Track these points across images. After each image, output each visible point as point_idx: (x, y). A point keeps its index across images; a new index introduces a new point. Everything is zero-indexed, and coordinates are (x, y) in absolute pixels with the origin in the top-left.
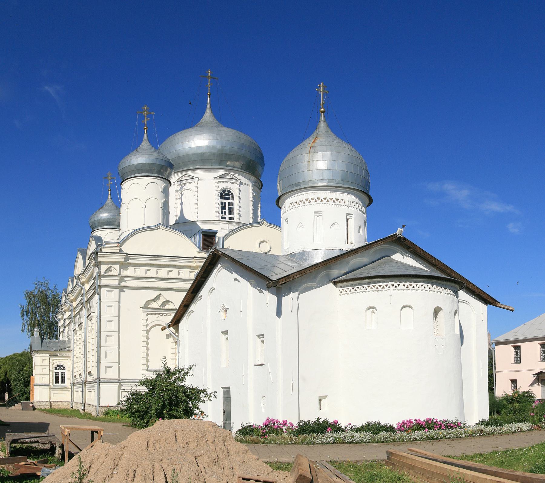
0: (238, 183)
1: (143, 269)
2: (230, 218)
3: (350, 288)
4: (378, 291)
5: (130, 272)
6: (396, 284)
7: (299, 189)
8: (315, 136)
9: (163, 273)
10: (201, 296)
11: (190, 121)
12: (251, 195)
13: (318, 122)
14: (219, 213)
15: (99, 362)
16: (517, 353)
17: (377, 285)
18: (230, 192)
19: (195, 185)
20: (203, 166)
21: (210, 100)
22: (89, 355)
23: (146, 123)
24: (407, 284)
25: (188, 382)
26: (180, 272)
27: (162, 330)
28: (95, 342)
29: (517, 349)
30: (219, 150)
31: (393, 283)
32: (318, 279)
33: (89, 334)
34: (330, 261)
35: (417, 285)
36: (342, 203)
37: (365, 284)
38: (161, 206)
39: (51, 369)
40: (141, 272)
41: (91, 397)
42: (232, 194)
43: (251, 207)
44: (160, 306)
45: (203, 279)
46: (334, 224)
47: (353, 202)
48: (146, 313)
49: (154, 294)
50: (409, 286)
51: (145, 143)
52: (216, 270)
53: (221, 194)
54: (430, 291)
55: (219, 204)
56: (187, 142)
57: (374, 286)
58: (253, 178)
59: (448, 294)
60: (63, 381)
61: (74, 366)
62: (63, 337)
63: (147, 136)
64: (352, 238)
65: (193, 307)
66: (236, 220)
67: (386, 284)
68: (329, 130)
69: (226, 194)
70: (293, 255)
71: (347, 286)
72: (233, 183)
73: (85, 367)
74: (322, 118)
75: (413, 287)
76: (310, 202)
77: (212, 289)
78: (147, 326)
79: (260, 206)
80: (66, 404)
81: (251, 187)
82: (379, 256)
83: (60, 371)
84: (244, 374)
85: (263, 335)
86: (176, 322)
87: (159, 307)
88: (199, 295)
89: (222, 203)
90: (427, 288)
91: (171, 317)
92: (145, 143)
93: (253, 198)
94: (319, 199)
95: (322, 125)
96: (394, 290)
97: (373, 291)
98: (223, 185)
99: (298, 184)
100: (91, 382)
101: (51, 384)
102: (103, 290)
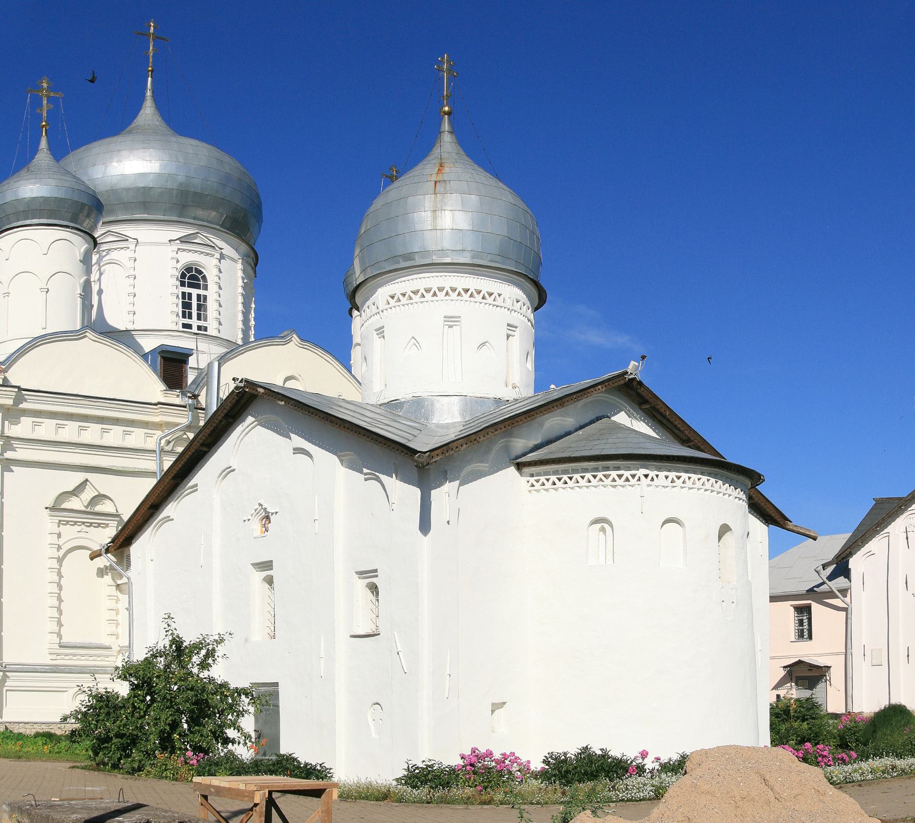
0: (217, 255)
1: (51, 423)
2: (199, 328)
3: (553, 478)
4: (614, 487)
5: (23, 428)
6: (652, 474)
7: (396, 270)
8: (437, 161)
9: (92, 434)
10: (196, 485)
11: (113, 122)
12: (240, 283)
13: (438, 132)
14: (177, 315)
16: (801, 623)
17: (614, 474)
18: (200, 272)
19: (128, 253)
20: (146, 216)
21: (152, 82)
23: (45, 114)
24: (672, 475)
25: (219, 672)
26: (126, 433)
27: (92, 559)
29: (804, 611)
30: (181, 184)
31: (646, 472)
32: (492, 456)
34: (514, 421)
35: (689, 478)
36: (499, 302)
37: (586, 470)
38: (79, 291)
40: (47, 429)
42: (204, 278)
43: (240, 307)
44: (87, 507)
45: (205, 449)
46: (483, 344)
47: (518, 302)
48: (56, 520)
49: (73, 479)
50: (675, 479)
51: (43, 156)
52: (239, 429)
53: (183, 276)
54: (712, 491)
55: (178, 297)
56: (115, 164)
57: (537, 481)
58: (244, 247)
59: (740, 499)
63: (49, 143)
65: (170, 510)
66: (211, 331)
67: (633, 472)
68: (462, 153)
69: (192, 277)
70: (396, 405)
71: (546, 474)
72: (207, 254)
74: (446, 126)
75: (639, 480)
76: (435, 294)
77: (229, 470)
78: (59, 548)
79: (253, 306)
81: (239, 266)
82: (591, 416)
84: (322, 654)
85: (376, 571)
86: (123, 542)
87: (83, 509)
88: (191, 483)
89: (184, 294)
90: (699, 484)
92: (43, 156)
93: (244, 288)
94: (454, 290)
95: (447, 141)
96: (649, 486)
97: (604, 486)
98: (187, 258)
99: (409, 257)
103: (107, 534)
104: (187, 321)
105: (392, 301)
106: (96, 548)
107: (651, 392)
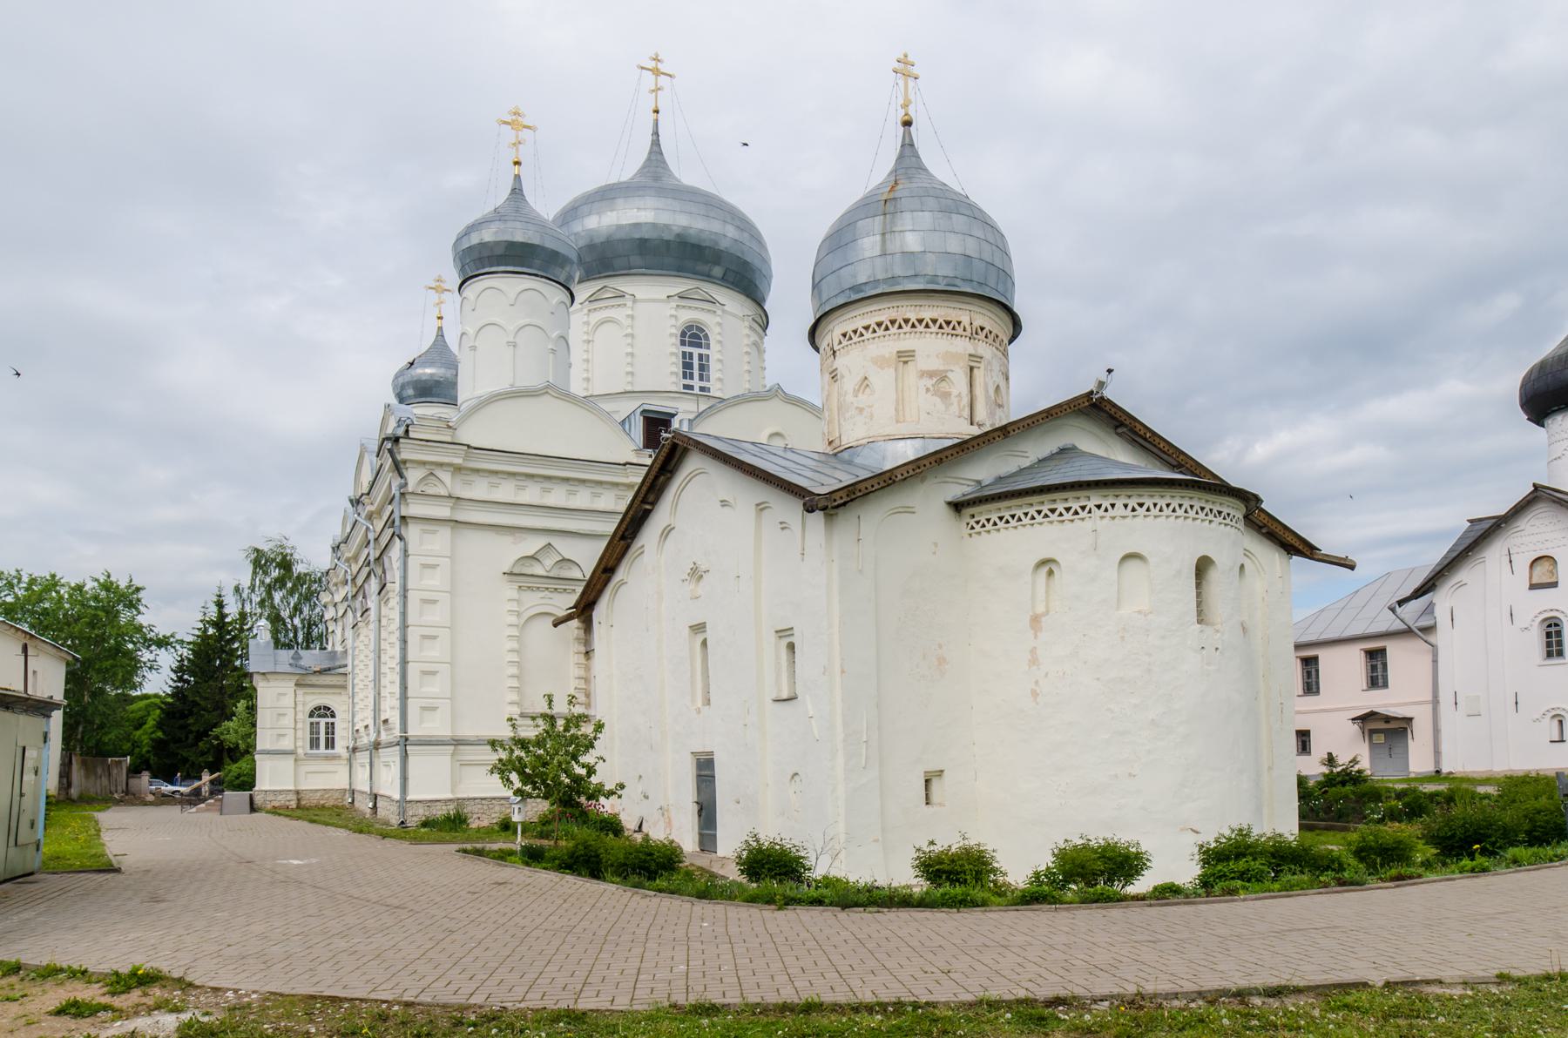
2: (702, 389)
15: (404, 697)
22: (384, 681)
28: (396, 651)
29: (1376, 657)
33: (384, 634)
36: (959, 330)
39: (300, 716)
40: (506, 491)
41: (388, 784)
42: (706, 336)
48: (516, 586)
49: (532, 545)
53: (683, 334)
60: (330, 743)
61: (355, 712)
62: (335, 644)
64: (981, 413)
69: (693, 336)
73: (377, 710)
77: (667, 531)
80: (337, 795)
83: (323, 721)
89: (684, 353)
91: (572, 599)
98: (687, 316)
100: (390, 745)
101: (300, 751)
102: (412, 532)
103: (565, 602)
104: (688, 382)
105: (845, 343)
106: (562, 613)
107: (1115, 405)
